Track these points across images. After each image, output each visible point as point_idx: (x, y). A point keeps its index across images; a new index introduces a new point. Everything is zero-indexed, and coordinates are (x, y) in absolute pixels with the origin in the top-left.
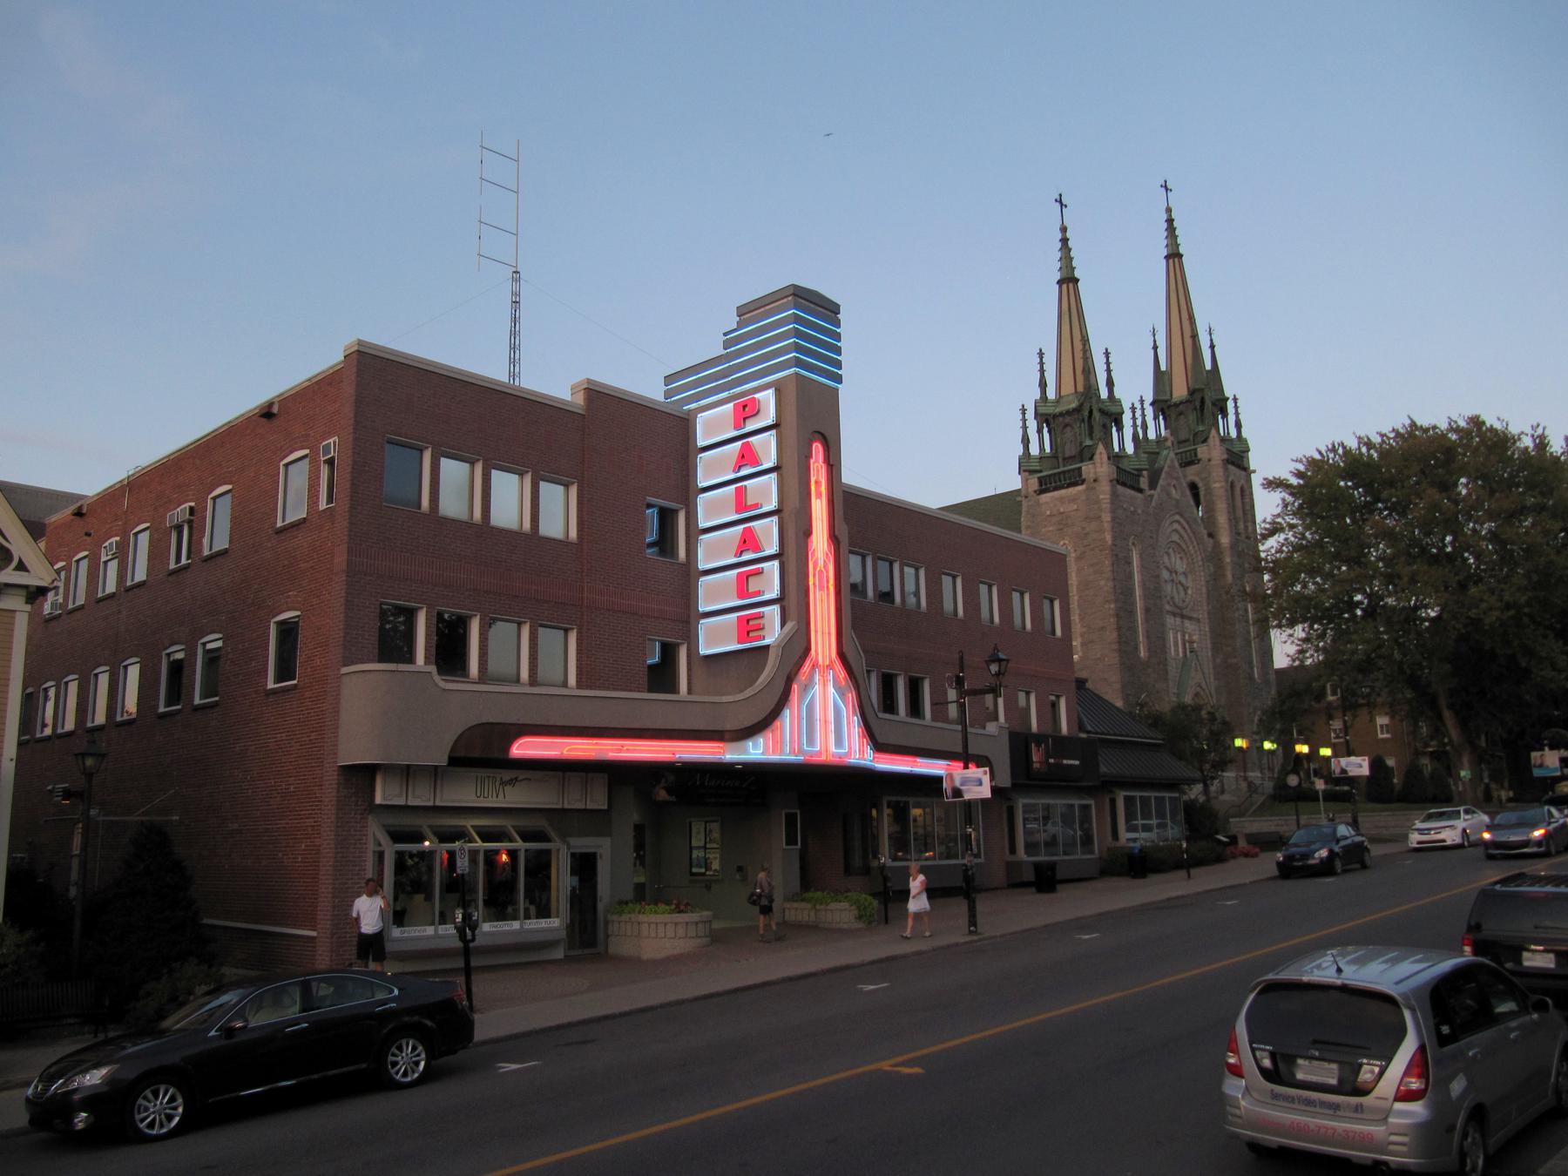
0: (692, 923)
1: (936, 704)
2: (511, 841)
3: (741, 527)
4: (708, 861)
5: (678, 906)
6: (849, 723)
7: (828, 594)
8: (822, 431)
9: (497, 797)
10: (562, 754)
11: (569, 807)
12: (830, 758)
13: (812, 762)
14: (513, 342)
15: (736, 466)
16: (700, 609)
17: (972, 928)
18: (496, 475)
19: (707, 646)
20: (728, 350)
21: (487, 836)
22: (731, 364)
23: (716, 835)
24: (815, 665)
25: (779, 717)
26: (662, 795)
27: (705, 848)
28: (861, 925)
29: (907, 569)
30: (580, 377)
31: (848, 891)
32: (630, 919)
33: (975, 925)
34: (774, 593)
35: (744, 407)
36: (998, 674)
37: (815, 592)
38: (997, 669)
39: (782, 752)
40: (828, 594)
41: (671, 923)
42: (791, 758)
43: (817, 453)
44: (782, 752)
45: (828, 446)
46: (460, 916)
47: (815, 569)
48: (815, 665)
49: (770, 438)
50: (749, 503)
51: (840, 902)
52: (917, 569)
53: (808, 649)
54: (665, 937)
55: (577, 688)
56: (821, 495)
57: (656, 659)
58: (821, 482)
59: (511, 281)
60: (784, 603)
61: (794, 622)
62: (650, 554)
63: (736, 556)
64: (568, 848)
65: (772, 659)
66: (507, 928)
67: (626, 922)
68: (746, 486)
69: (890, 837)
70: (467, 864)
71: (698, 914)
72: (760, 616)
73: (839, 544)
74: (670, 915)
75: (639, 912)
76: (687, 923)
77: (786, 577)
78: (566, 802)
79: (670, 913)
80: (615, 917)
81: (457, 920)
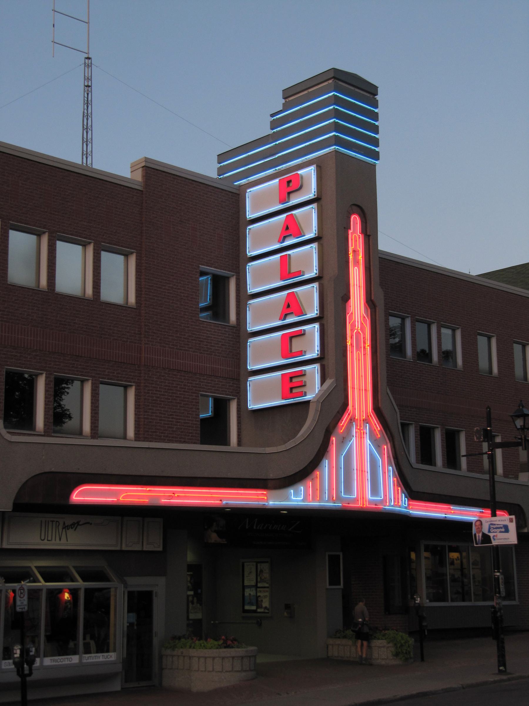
0: (220, 657)
1: (471, 455)
2: (72, 581)
3: (285, 293)
4: (259, 599)
5: (225, 641)
6: (384, 473)
7: (365, 355)
8: (358, 204)
9: (60, 539)
10: (118, 500)
11: (147, 550)
12: (366, 505)
13: (349, 509)
14: (85, 123)
15: (280, 238)
16: (248, 367)
17: (501, 668)
18: (60, 245)
19: (255, 402)
20: (275, 130)
21: (49, 576)
22: (277, 143)
23: (266, 575)
24: (352, 420)
25: (319, 467)
26: (214, 538)
27: (256, 586)
28: (397, 662)
29: (444, 331)
30: (138, 155)
31: (386, 629)
32: (182, 653)
33: (504, 665)
34: (315, 353)
35: (289, 182)
36: (523, 428)
37: (352, 352)
38: (522, 424)
39: (321, 499)
40: (365, 355)
41: (220, 657)
42: (330, 505)
43: (355, 223)
44: (321, 499)
45: (366, 220)
46: (18, 652)
47: (352, 330)
48: (352, 420)
49: (312, 210)
50: (293, 270)
51: (379, 639)
52: (454, 330)
53: (345, 405)
54: (213, 670)
55: (136, 440)
56: (358, 262)
57: (210, 414)
58: (358, 251)
59: (84, 65)
60: (325, 362)
61: (333, 380)
62: (203, 317)
63: (280, 319)
64: (126, 587)
65: (312, 413)
66: (67, 662)
67: (178, 656)
68: (289, 255)
69: (428, 578)
70: (26, 602)
71: (244, 649)
72: (302, 374)
73: (375, 308)
74: (218, 650)
75: (190, 647)
76: (233, 658)
77: (326, 338)
78: (124, 545)
79: (217, 648)
80: (169, 652)
81: (16, 656)
